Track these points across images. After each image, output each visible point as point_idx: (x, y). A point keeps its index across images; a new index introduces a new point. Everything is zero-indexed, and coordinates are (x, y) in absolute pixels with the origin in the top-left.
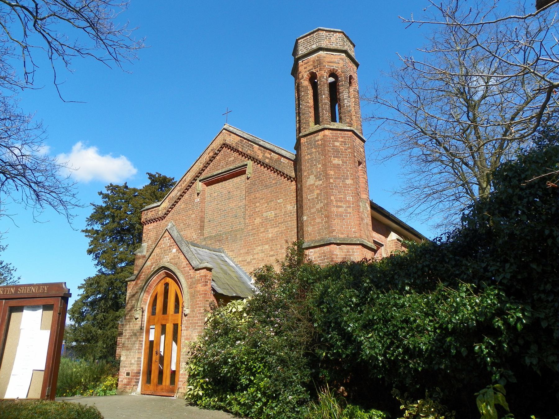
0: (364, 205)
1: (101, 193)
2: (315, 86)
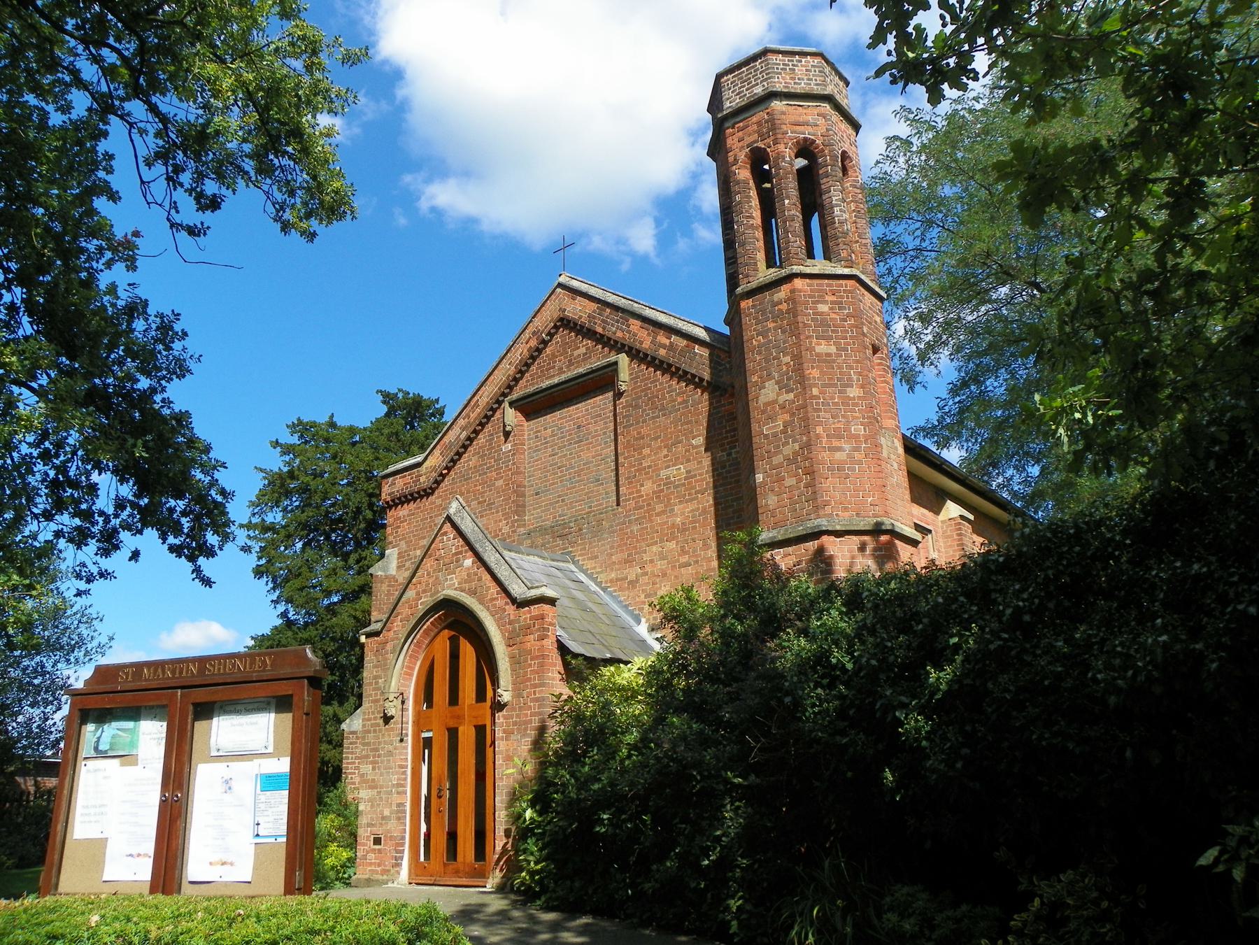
0: (889, 444)
1: (276, 444)
2: (761, 176)
